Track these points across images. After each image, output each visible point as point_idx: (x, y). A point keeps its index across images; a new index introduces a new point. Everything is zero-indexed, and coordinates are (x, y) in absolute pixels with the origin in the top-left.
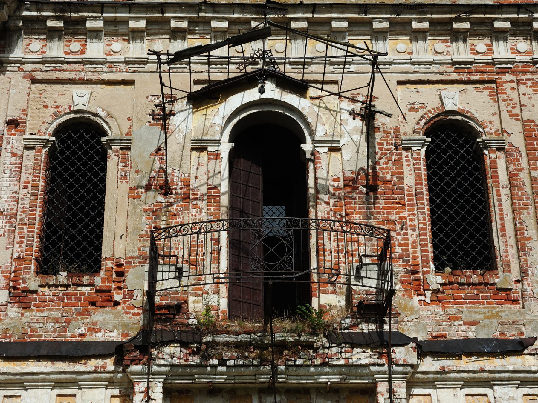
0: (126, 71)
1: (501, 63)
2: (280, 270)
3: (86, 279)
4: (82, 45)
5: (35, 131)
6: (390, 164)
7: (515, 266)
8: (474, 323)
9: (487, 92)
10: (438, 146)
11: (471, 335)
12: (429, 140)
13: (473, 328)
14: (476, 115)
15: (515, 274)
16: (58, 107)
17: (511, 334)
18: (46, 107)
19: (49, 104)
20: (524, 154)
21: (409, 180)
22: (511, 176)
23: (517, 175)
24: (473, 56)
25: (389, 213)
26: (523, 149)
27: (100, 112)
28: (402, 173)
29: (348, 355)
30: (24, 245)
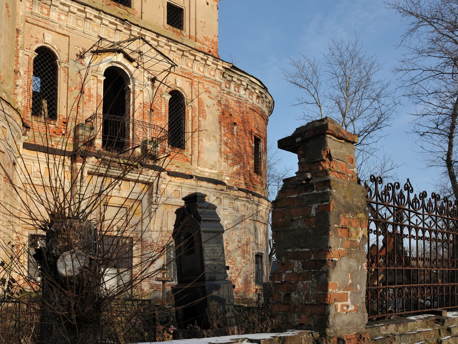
0: (66, 31)
1: (206, 78)
2: (397, 214)
3: (52, 122)
4: (48, 11)
5: (28, 48)
6: (158, 103)
7: (190, 150)
8: (177, 167)
9: (189, 83)
10: (40, 59)
11: (177, 171)
12: (37, 54)
13: (178, 169)
14: (185, 91)
15: (190, 153)
16: (37, 38)
17: (188, 173)
18: (32, 37)
19: (34, 36)
20: (197, 110)
21: (163, 111)
22: (193, 117)
23: (194, 117)
24: (186, 67)
25: (157, 121)
26: (197, 108)
27: (55, 47)
28: (161, 107)
29: (147, 172)
30: (26, 100)
